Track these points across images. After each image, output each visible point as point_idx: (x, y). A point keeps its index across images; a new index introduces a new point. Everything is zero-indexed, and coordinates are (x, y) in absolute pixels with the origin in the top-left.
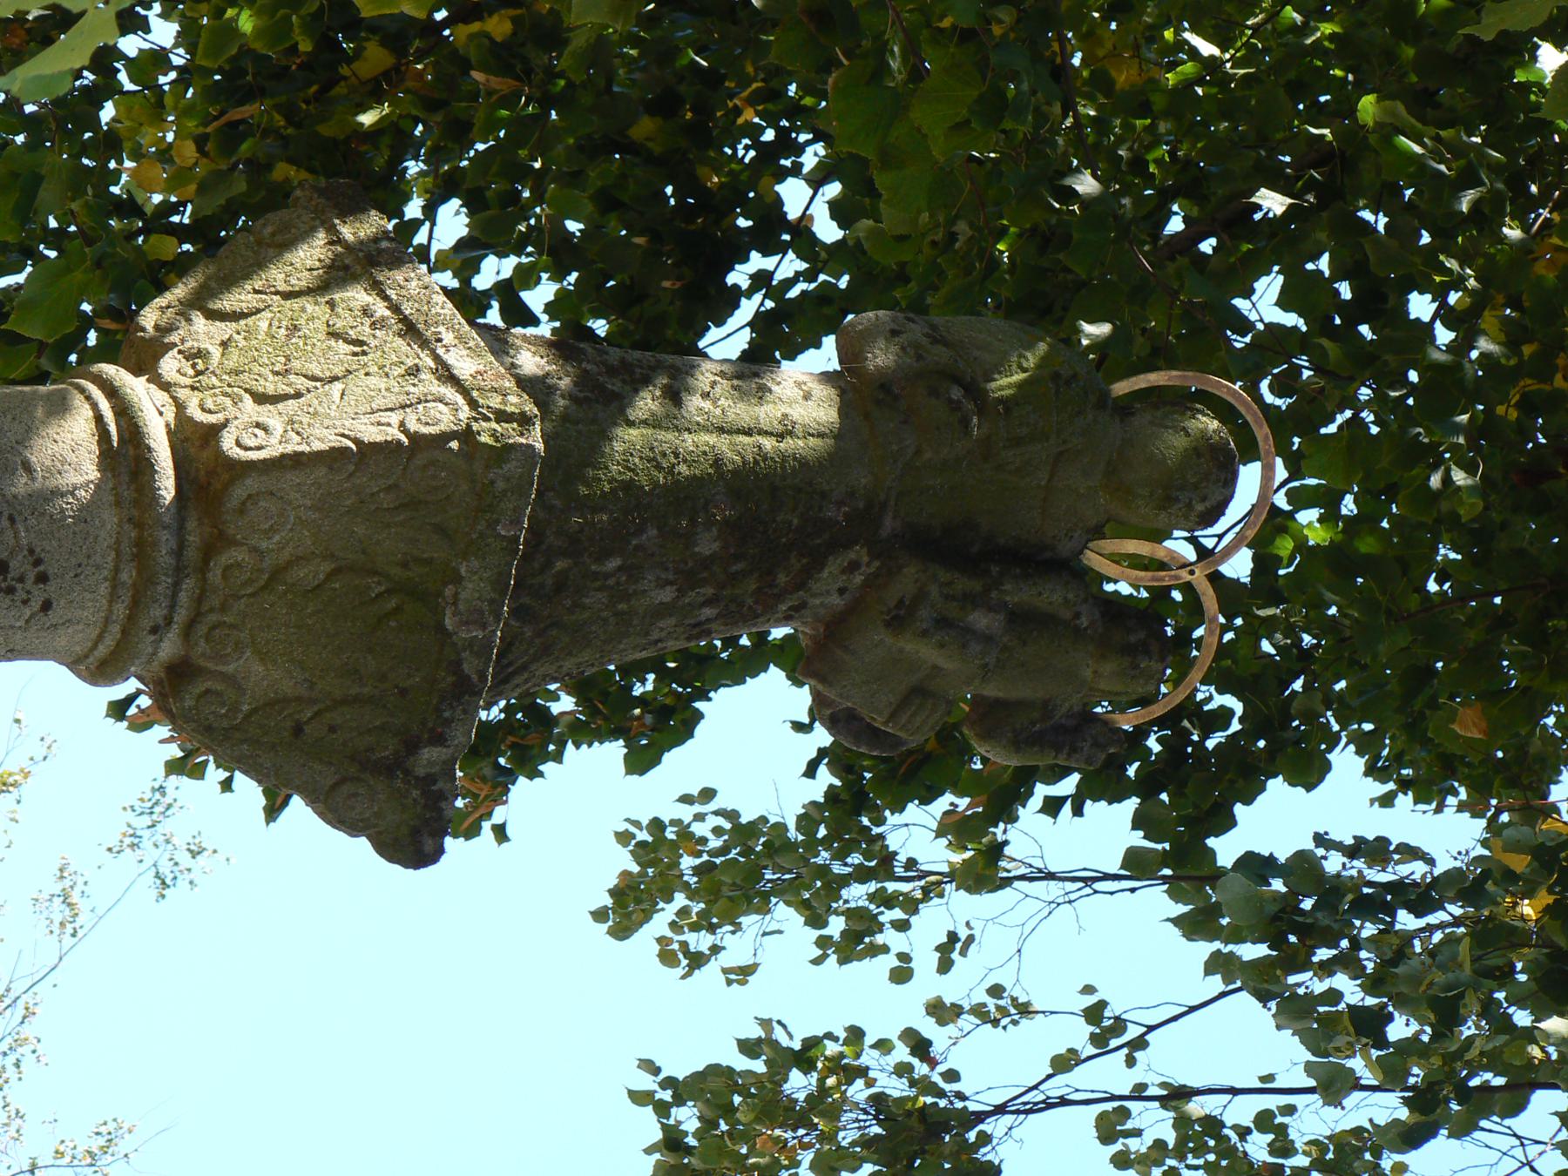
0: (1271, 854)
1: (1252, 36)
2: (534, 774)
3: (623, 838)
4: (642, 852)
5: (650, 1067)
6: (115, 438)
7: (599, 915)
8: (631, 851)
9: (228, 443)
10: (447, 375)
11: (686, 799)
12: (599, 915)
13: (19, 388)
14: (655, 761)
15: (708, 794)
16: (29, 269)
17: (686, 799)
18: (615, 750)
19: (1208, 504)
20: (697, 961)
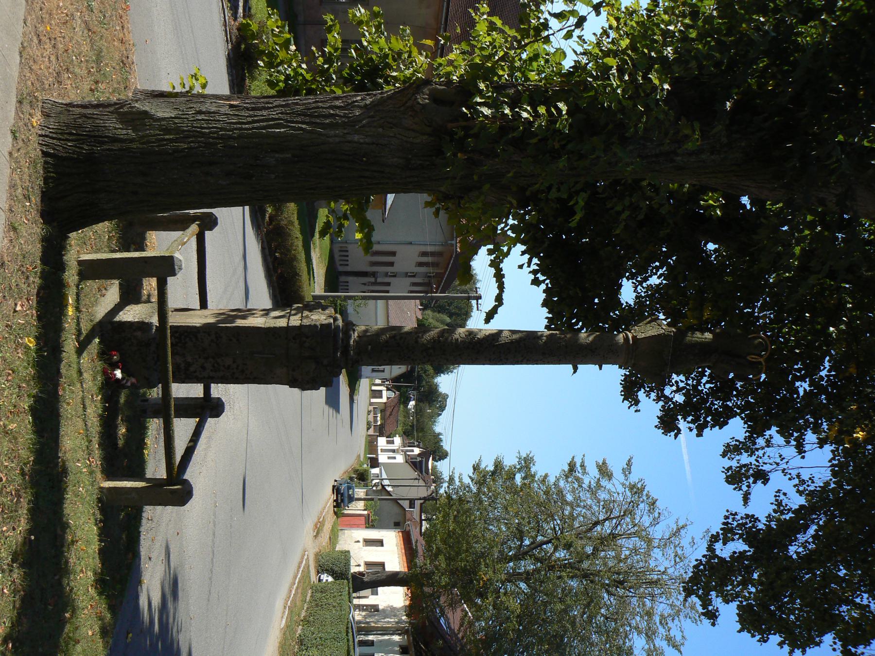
0: (494, 277)
1: (754, 312)
2: (545, 304)
3: (724, 446)
4: (726, 447)
5: (724, 468)
6: (689, 476)
7: (721, 455)
8: (491, 260)
9: (638, 337)
10: (662, 328)
11: (731, 439)
12: (721, 455)
13: (300, 125)
14: (722, 428)
15: (734, 438)
16: (850, 647)
17: (731, 439)
18: (717, 427)
19: (319, 226)
20: (733, 459)
